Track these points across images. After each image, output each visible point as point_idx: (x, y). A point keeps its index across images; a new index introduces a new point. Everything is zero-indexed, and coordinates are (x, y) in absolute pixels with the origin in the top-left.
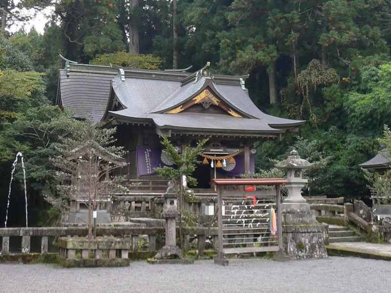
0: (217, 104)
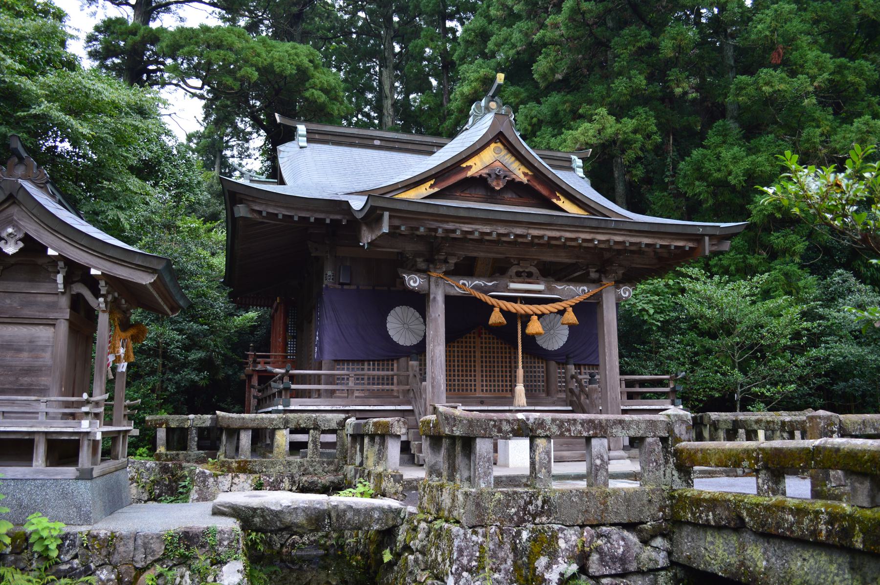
0: (525, 180)
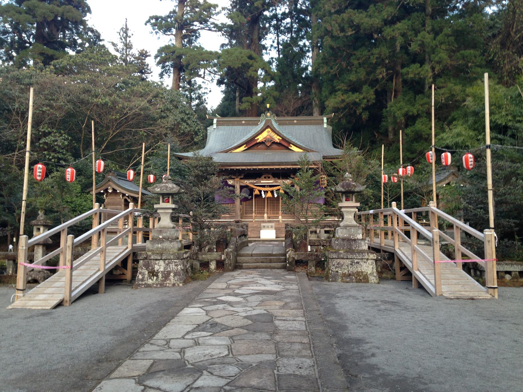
0: (278, 141)
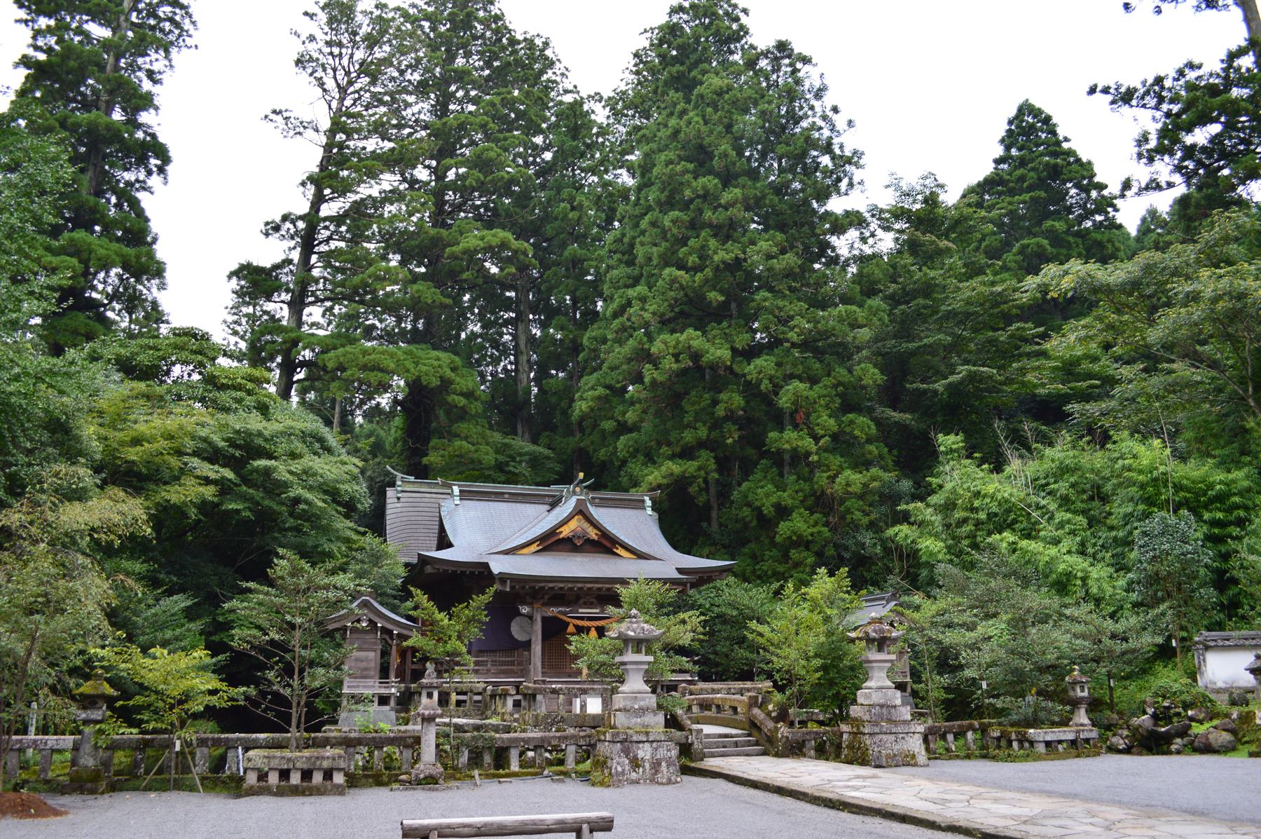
0: (596, 538)
